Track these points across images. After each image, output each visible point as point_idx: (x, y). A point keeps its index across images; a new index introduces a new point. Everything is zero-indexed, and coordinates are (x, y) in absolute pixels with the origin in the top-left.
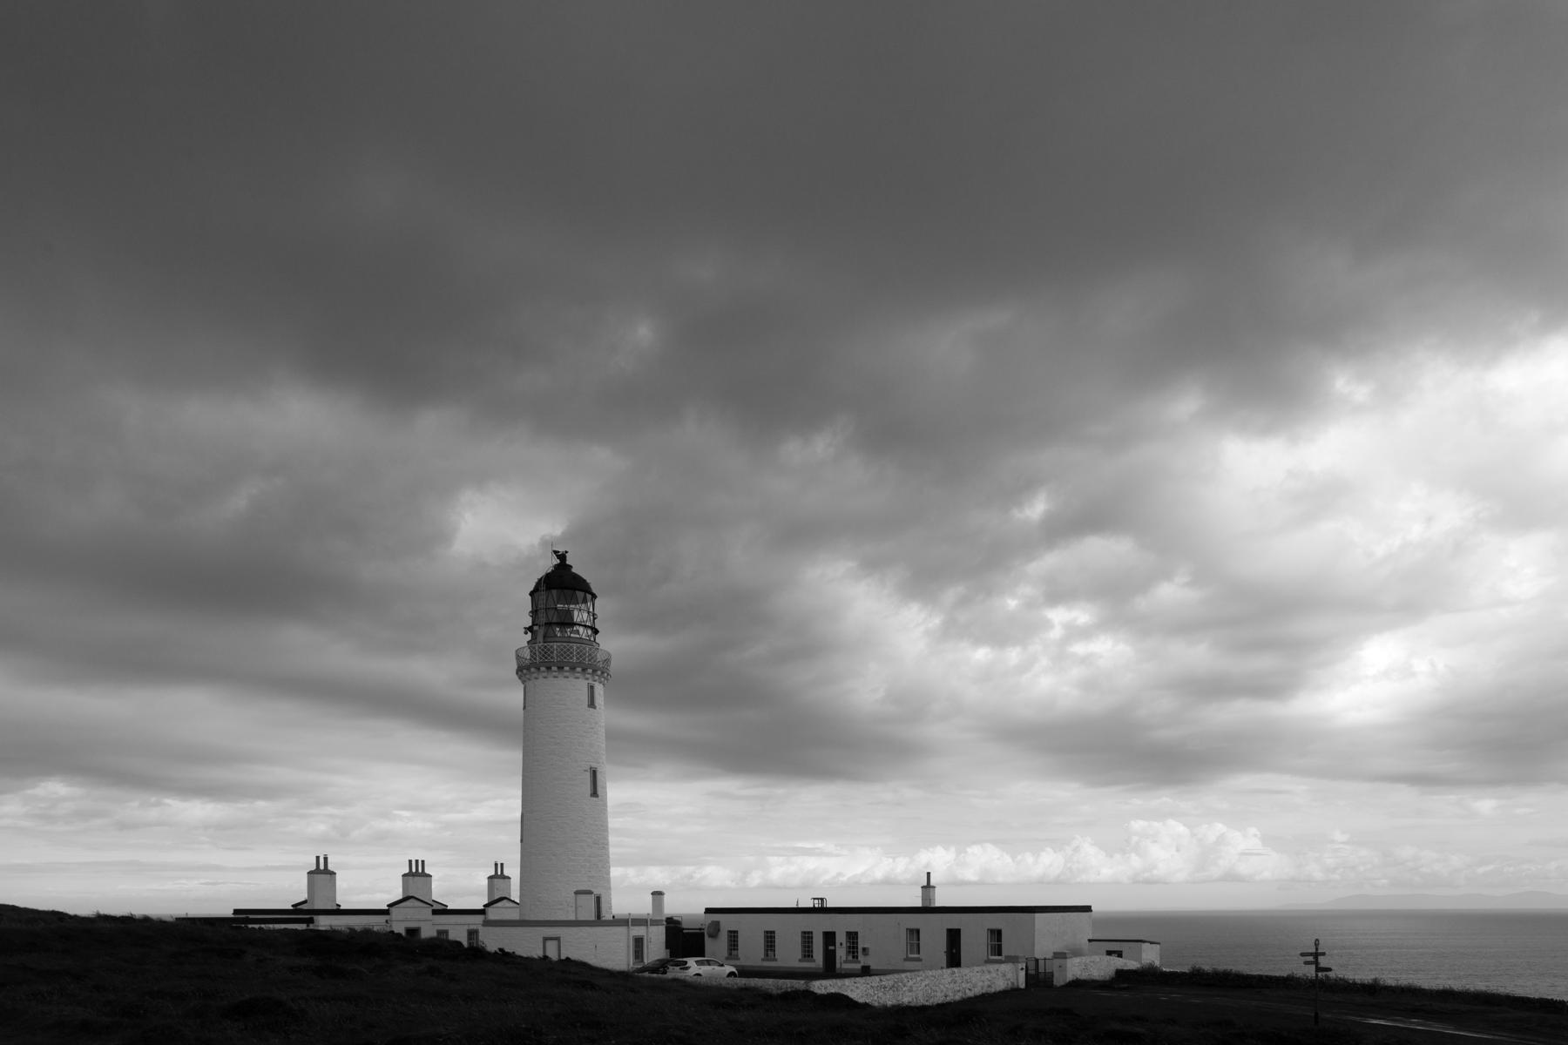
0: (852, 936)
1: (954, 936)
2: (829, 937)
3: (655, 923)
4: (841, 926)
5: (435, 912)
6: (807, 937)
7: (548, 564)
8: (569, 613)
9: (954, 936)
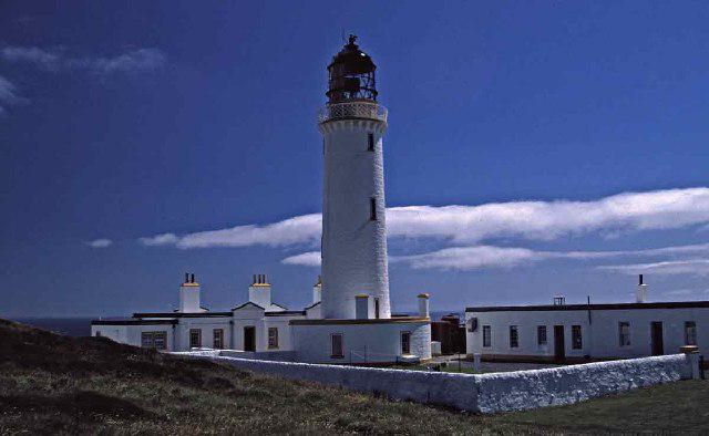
0: (576, 330)
1: (657, 328)
2: (559, 330)
3: (686, 331)
4: (568, 321)
5: (267, 314)
6: (542, 330)
7: (339, 47)
8: (357, 82)
9: (657, 328)
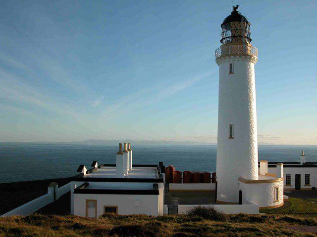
7: (228, 12)
